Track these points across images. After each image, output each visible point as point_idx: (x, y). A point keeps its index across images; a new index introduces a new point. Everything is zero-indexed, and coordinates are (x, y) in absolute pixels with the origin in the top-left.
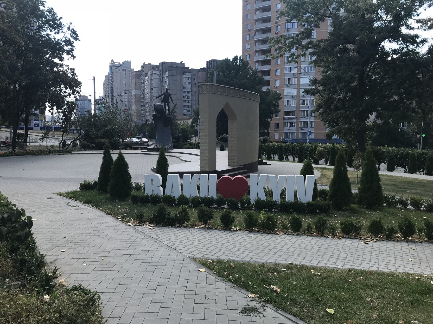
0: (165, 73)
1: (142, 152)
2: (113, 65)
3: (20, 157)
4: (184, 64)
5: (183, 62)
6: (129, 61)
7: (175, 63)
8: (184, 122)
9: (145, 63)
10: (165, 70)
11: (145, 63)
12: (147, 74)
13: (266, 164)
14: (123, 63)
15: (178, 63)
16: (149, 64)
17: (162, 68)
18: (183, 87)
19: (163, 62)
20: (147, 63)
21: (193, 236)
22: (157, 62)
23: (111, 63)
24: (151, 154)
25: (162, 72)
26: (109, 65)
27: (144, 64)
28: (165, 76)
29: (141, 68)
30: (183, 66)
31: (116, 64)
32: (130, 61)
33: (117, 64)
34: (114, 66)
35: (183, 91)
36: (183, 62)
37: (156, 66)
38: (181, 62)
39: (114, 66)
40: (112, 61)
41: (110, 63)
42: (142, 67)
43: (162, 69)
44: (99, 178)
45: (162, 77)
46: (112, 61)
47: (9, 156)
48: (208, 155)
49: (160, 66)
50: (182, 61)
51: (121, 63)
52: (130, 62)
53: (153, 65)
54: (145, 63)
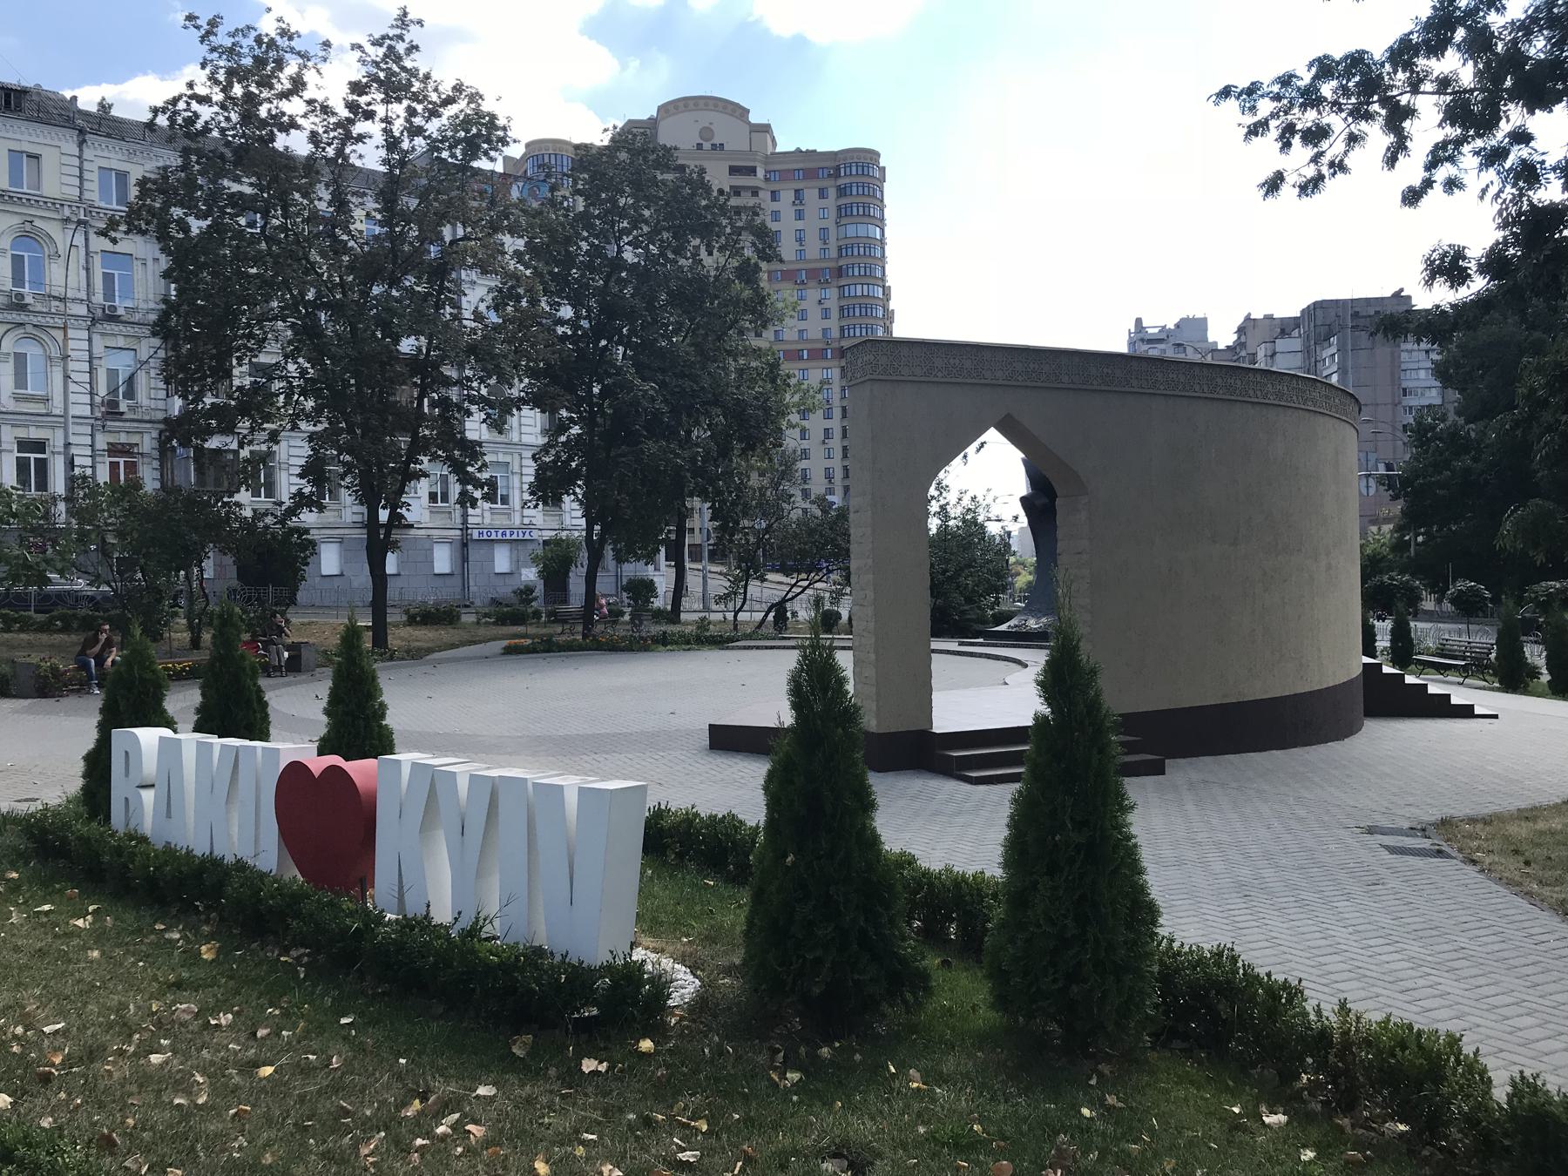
0: (1326, 344)
1: (961, 644)
2: (1141, 335)
3: (571, 656)
4: (1409, 298)
5: (1403, 294)
6: (1199, 315)
7: (1368, 300)
8: (1379, 529)
9: (1249, 314)
10: (1323, 330)
11: (1252, 317)
12: (1255, 354)
13: (1442, 708)
14: (1177, 326)
15: (1382, 298)
16: (1269, 318)
17: (1312, 324)
18: (1405, 390)
19: (1315, 304)
20: (1258, 314)
21: (1511, 1033)
22: (1290, 307)
23: (1133, 330)
24: (988, 656)
25: (1313, 342)
26: (1127, 338)
27: (1248, 318)
28: (1327, 353)
29: (1235, 337)
30: (1405, 308)
31: (1150, 331)
32: (1202, 316)
33: (1156, 330)
34: (1142, 340)
35: (1404, 407)
36: (1403, 294)
37: (1295, 323)
38: (1397, 295)
39: (1142, 340)
40: (1139, 321)
41: (1130, 333)
42: (1241, 330)
43: (1312, 329)
44: (381, 711)
45: (1313, 360)
46: (1139, 321)
47: (538, 652)
48: (873, 656)
49: (1304, 319)
50: (1402, 290)
51: (1171, 326)
52: (1205, 320)
53: (1282, 319)
54: (1249, 314)
